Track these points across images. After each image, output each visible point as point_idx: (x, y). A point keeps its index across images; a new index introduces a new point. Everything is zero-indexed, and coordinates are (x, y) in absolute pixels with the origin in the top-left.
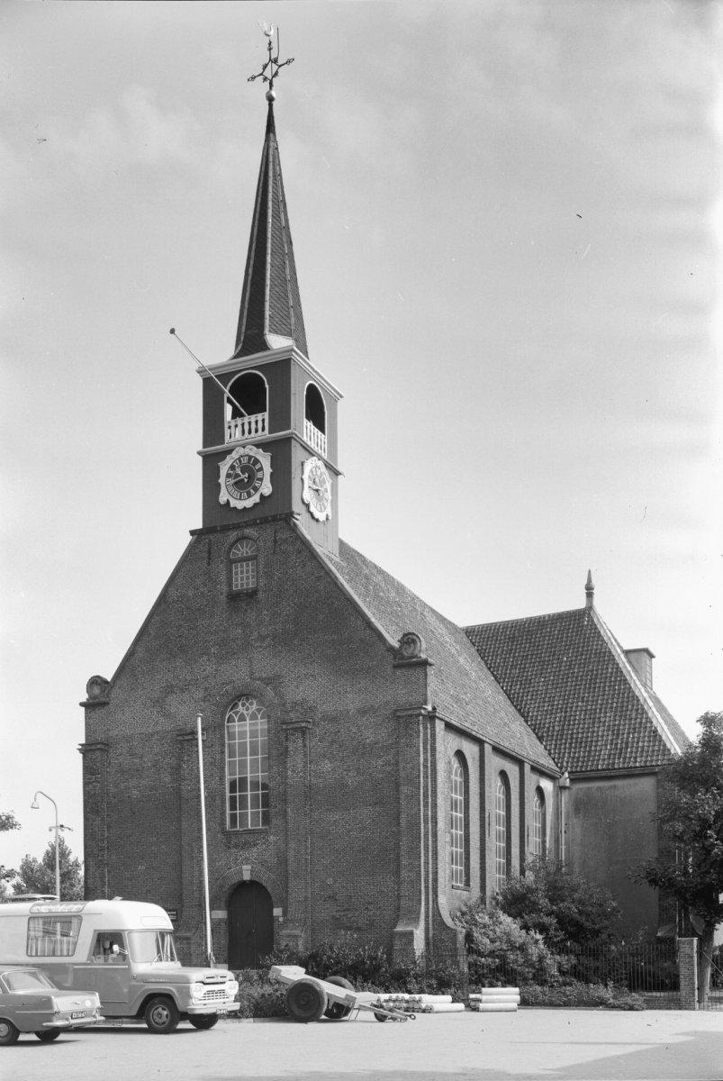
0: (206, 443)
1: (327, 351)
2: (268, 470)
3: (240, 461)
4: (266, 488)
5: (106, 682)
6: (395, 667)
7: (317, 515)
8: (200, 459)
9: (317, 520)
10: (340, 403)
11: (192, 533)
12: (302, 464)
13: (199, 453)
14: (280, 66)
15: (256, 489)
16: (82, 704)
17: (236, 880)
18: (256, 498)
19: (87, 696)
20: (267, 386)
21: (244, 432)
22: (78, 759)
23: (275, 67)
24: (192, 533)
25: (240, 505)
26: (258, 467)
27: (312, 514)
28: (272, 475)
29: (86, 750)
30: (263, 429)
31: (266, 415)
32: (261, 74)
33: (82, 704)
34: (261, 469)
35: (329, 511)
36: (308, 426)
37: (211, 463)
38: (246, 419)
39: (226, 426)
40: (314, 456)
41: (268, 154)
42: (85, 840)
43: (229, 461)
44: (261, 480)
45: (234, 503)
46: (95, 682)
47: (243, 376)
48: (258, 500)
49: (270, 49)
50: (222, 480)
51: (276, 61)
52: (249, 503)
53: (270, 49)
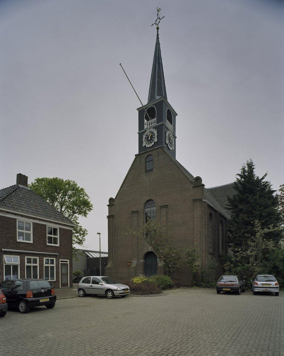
0: (139, 130)
1: (174, 99)
2: (156, 135)
3: (149, 143)
4: (156, 140)
5: (113, 199)
6: (193, 187)
7: (170, 148)
8: (138, 112)
9: (170, 150)
10: (177, 117)
11: (136, 155)
12: (166, 133)
13: (138, 133)
14: (160, 19)
15: (153, 141)
16: (107, 205)
17: (146, 251)
18: (153, 143)
19: (109, 203)
20: (156, 110)
21: (150, 124)
22: (106, 220)
23: (159, 20)
24: (136, 155)
25: (148, 146)
26: (154, 136)
27: (168, 147)
28: (157, 136)
29: (108, 217)
30: (155, 123)
31: (156, 119)
32: (155, 23)
33: (107, 205)
34: (154, 134)
35: (173, 147)
36: (167, 122)
37: (141, 135)
38: (150, 121)
39: (145, 124)
40: (169, 130)
41: (156, 47)
42: (108, 224)
43: (146, 134)
44: (154, 138)
45: (147, 146)
46: (111, 200)
47: (148, 109)
48: (153, 144)
49: (158, 15)
50: (144, 140)
51: (159, 18)
52: (151, 145)
53: (158, 15)
